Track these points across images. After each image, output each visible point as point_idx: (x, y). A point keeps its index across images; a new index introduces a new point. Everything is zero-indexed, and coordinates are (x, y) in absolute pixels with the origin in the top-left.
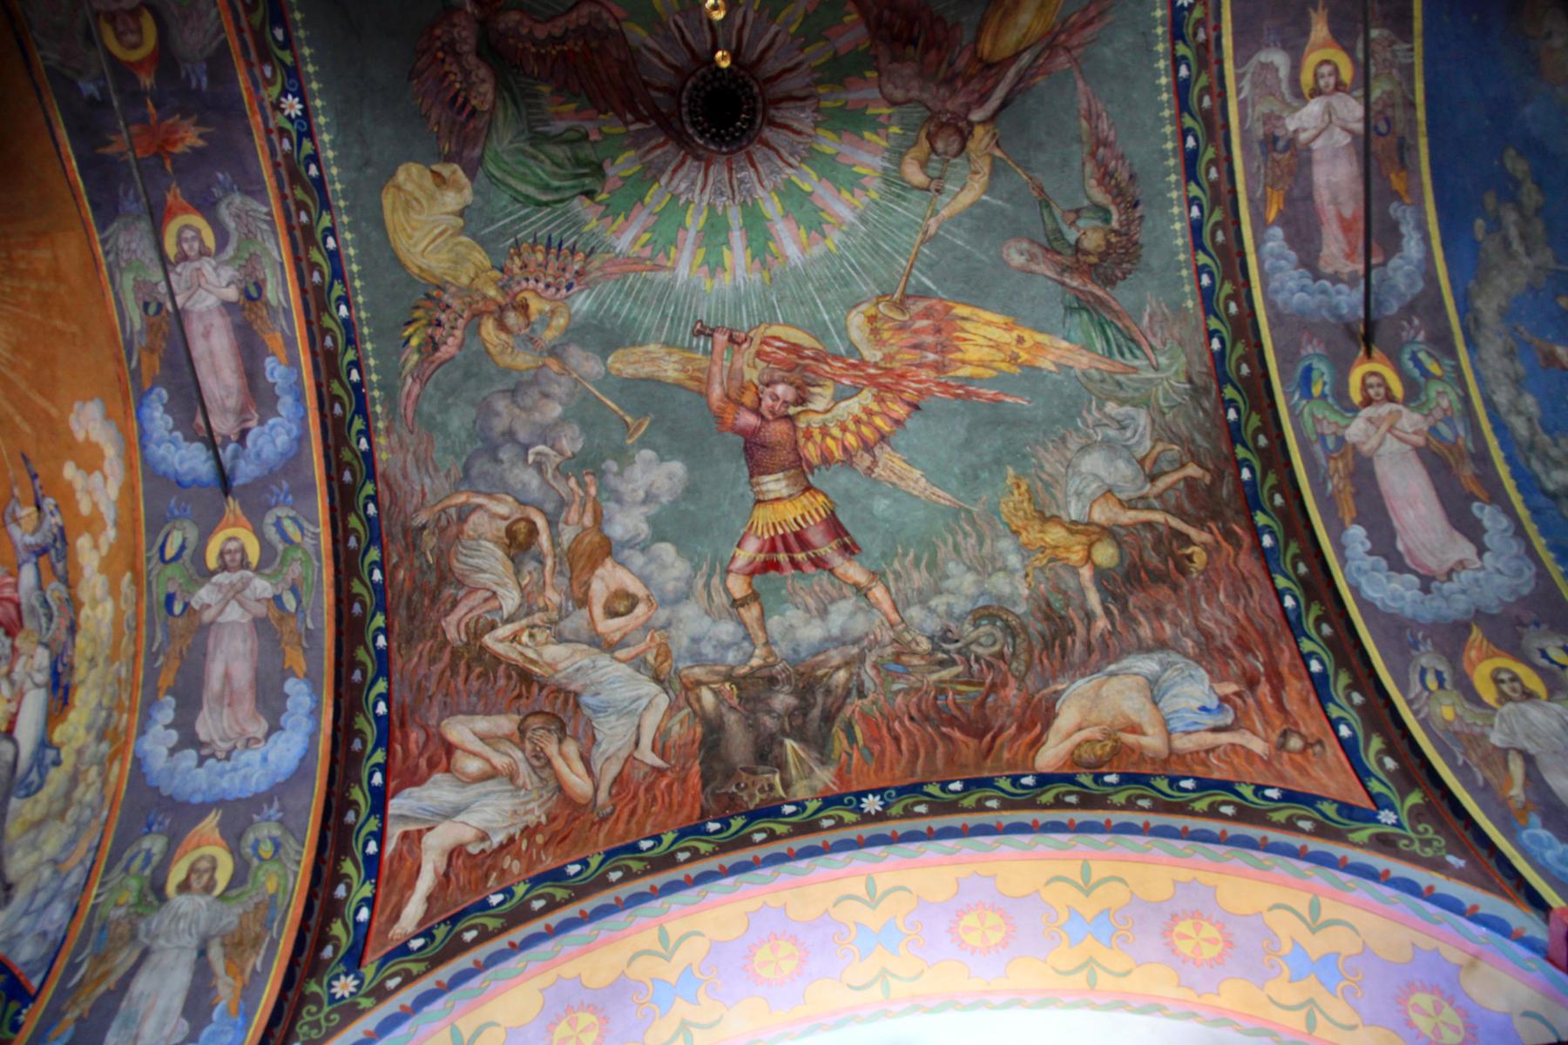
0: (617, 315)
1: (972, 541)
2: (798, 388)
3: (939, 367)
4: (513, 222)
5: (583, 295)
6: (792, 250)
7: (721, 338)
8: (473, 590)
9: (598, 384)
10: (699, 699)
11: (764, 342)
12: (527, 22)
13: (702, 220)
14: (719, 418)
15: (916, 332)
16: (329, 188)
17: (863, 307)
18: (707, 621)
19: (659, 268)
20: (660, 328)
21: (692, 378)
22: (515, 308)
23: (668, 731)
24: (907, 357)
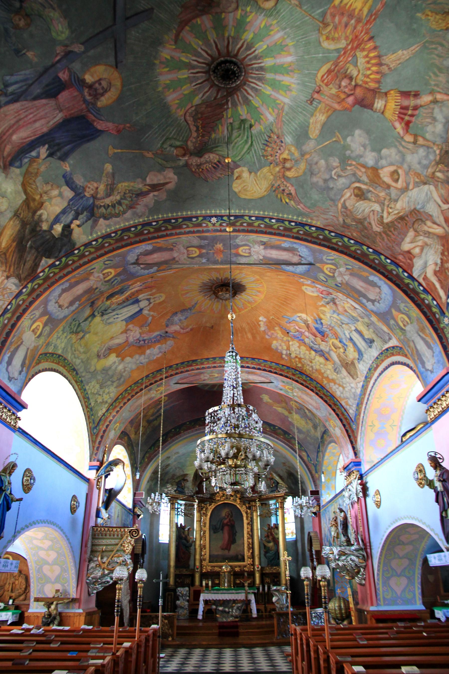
0: (296, 129)
1: (440, 48)
2: (345, 77)
3: (359, 21)
4: (256, 156)
5: (286, 138)
6: (289, 59)
7: (316, 96)
8: (369, 216)
9: (318, 145)
10: (438, 178)
11: (323, 81)
12: (191, 139)
13: (269, 88)
14: (346, 109)
15: (340, 22)
16: (238, 214)
17: (321, 40)
18: (415, 155)
19: (283, 109)
20: (305, 116)
21: (328, 111)
22: (284, 163)
23: (442, 195)
24: (349, 31)
